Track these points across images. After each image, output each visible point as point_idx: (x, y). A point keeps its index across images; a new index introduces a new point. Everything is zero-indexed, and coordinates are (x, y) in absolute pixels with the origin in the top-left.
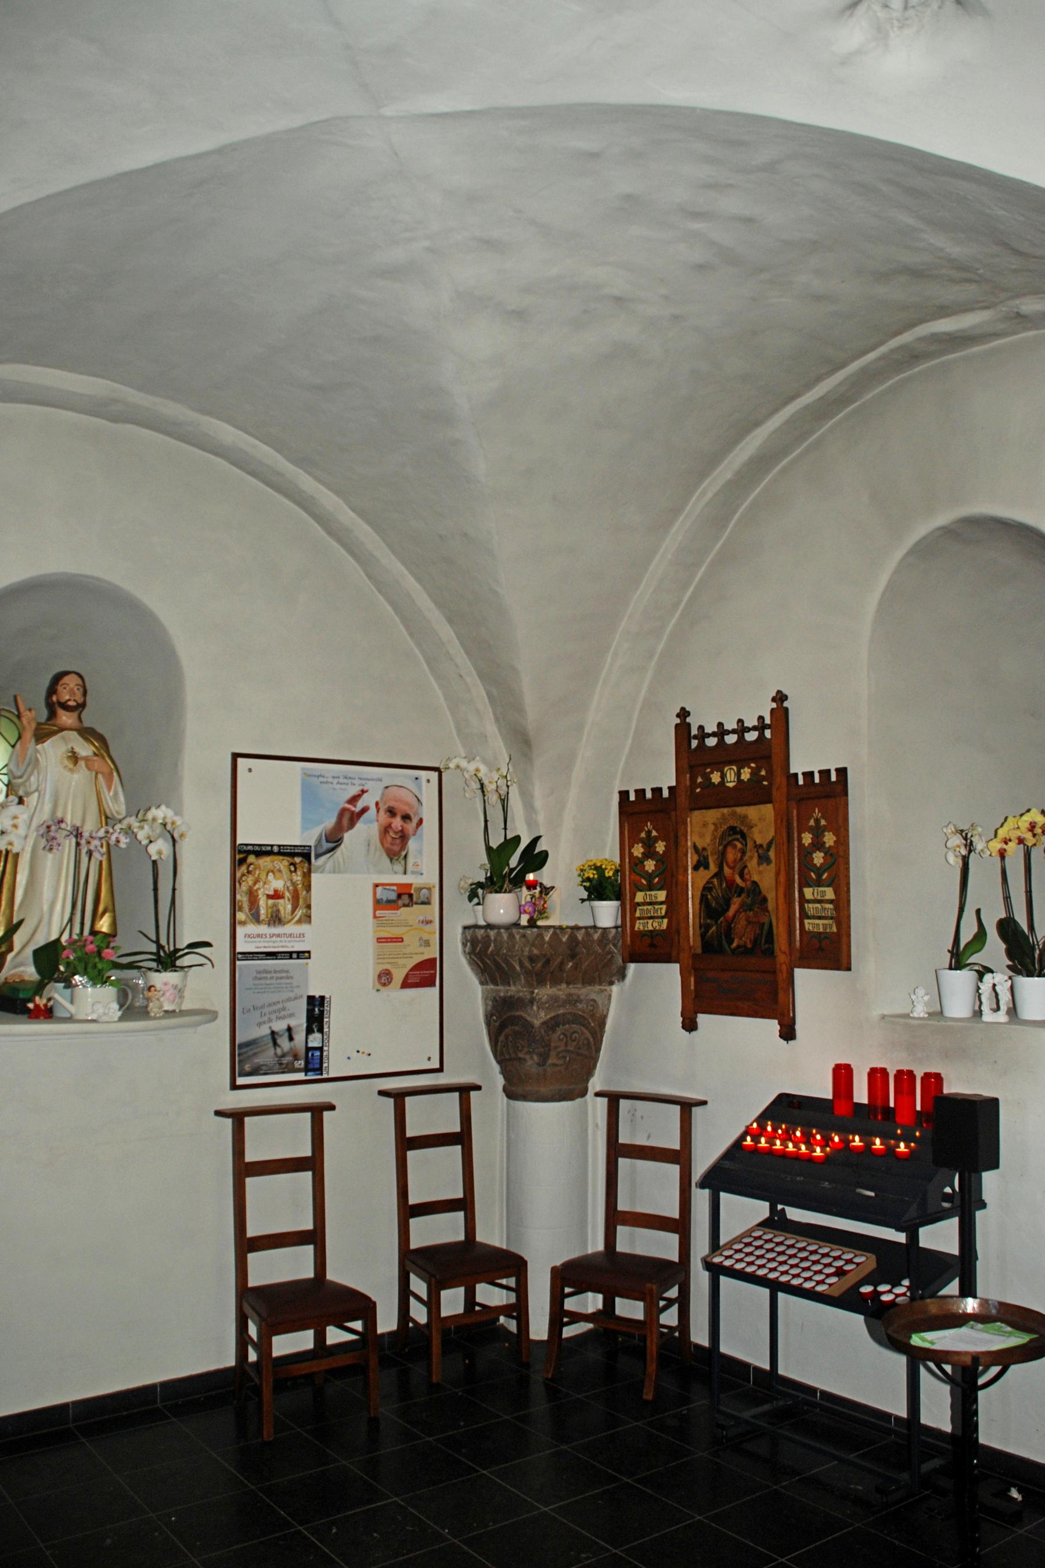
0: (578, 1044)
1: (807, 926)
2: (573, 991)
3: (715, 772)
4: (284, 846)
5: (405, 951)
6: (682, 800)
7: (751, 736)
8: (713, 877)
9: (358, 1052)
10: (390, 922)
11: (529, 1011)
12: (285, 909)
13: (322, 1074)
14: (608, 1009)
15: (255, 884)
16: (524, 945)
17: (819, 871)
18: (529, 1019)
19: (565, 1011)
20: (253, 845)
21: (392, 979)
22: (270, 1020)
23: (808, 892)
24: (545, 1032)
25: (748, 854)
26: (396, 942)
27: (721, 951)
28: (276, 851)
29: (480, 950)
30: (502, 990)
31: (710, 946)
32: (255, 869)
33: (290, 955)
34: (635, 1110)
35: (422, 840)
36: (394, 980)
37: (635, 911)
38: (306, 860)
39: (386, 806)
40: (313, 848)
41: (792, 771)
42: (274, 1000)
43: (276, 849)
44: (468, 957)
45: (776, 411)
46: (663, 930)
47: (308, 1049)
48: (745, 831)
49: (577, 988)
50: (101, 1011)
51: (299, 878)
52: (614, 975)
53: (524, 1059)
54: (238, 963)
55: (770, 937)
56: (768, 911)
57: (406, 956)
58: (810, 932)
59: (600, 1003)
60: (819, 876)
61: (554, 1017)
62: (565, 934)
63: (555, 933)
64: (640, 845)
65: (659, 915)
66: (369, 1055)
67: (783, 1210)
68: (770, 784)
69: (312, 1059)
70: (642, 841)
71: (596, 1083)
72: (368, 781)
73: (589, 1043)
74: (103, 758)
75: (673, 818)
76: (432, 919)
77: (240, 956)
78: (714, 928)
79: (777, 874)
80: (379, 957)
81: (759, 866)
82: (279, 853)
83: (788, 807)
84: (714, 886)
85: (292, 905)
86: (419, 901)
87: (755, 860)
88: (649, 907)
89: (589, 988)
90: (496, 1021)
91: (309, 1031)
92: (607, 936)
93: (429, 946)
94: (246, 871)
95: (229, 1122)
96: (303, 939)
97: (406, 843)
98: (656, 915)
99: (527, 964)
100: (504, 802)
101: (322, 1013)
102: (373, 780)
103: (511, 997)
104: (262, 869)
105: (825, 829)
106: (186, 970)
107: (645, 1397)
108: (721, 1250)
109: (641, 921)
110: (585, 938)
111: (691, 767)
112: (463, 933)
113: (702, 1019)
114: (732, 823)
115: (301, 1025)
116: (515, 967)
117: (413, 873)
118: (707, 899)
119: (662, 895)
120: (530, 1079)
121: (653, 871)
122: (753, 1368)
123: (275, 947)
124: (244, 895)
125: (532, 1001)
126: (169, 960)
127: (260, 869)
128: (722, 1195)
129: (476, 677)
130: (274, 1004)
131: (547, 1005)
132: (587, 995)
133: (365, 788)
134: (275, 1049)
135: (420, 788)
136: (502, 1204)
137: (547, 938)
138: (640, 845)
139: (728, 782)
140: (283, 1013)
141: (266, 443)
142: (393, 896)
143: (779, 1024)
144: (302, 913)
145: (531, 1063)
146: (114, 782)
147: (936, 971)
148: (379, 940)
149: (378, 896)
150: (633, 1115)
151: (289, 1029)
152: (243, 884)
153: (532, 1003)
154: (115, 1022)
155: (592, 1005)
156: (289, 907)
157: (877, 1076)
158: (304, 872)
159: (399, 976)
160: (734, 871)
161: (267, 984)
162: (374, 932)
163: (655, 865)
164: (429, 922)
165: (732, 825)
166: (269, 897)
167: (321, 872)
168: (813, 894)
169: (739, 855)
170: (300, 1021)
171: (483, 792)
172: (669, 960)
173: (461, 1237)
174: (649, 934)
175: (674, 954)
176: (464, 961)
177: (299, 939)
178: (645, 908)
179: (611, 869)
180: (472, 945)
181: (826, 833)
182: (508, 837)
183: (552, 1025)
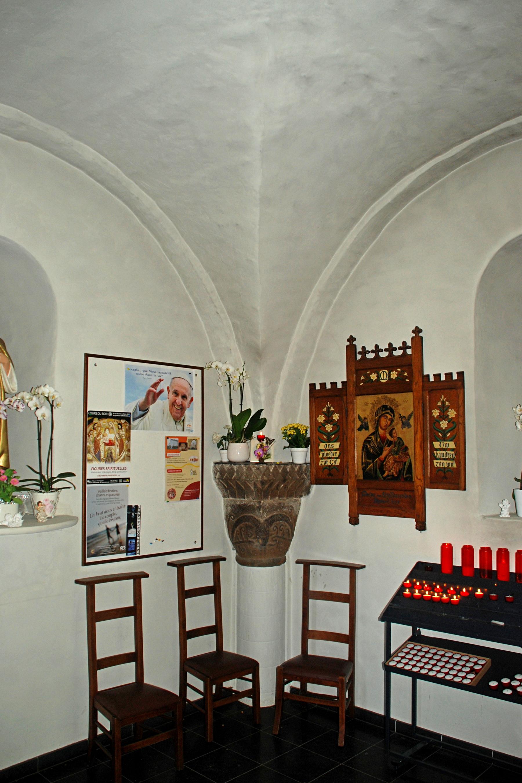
1: (435, 464)
2: (281, 501)
3: (373, 374)
4: (115, 412)
5: (183, 478)
6: (351, 389)
7: (398, 353)
8: (371, 435)
9: (157, 539)
10: (175, 460)
11: (257, 513)
12: (115, 452)
13: (136, 554)
14: (299, 511)
15: (98, 436)
16: (258, 474)
17: (444, 432)
18: (256, 518)
19: (277, 513)
20: (97, 412)
21: (175, 494)
22: (106, 521)
23: (436, 445)
24: (267, 526)
25: (395, 422)
26: (178, 472)
27: (376, 478)
28: (110, 416)
29: (226, 477)
30: (239, 501)
31: (367, 475)
32: (98, 426)
33: (118, 480)
34: (316, 570)
36: (176, 495)
37: (319, 454)
38: (128, 422)
39: (173, 390)
40: (132, 414)
41: (425, 373)
42: (109, 509)
43: (110, 414)
44: (217, 481)
45: (424, 162)
46: (337, 466)
47: (128, 539)
48: (393, 408)
49: (284, 499)
50: (11, 520)
51: (124, 433)
52: (303, 491)
53: (253, 542)
54: (87, 485)
55: (410, 470)
56: (409, 456)
57: (183, 481)
58: (437, 468)
59: (295, 508)
60: (444, 435)
62: (281, 467)
63: (275, 467)
64: (323, 415)
65: (335, 456)
66: (163, 541)
67: (419, 630)
68: (411, 381)
69: (131, 545)
70: (324, 413)
71: (291, 555)
72: (163, 374)
73: (289, 531)
74: (4, 353)
75: (345, 400)
76: (198, 458)
77: (89, 481)
78: (371, 465)
79: (415, 434)
80: (168, 481)
81: (402, 428)
82: (112, 417)
83: (423, 393)
84: (372, 440)
85: (119, 449)
86: (191, 448)
87: (400, 425)
88: (328, 452)
89: (290, 499)
90: (233, 519)
91: (129, 527)
92: (302, 469)
94: (92, 428)
95: (84, 587)
96: (126, 470)
97: (184, 412)
98: (333, 456)
99: (259, 485)
100: (242, 388)
101: (136, 516)
102: (166, 373)
103: (244, 505)
104: (102, 426)
105: (448, 407)
106: (59, 490)
107: (339, 745)
108: (393, 657)
109: (323, 460)
110: (291, 470)
111: (357, 371)
112: (214, 466)
113: (362, 518)
114: (384, 403)
115: (124, 524)
116: (250, 488)
117: (188, 430)
118: (367, 448)
119: (337, 445)
121: (331, 431)
122: (397, 722)
123: (108, 476)
124: (91, 443)
125: (259, 508)
126: (47, 485)
127: (100, 426)
128: (393, 624)
129: (226, 314)
130: (108, 511)
131: (268, 510)
132: (288, 504)
133: (162, 378)
134: (109, 539)
135: (191, 378)
136: (234, 626)
137: (271, 470)
138: (323, 415)
139: (382, 379)
140: (113, 517)
141: (112, 162)
142: (176, 444)
143: (416, 521)
144: (125, 454)
145: (257, 544)
146: (10, 370)
147: (513, 490)
148: (169, 471)
149: (168, 445)
150: (315, 573)
151: (117, 527)
152: (91, 436)
154: (20, 527)
156: (118, 450)
157: (486, 552)
158: (126, 429)
159: (179, 493)
160: (386, 431)
161: (104, 499)
162: (166, 466)
164: (196, 460)
165: (385, 404)
166: (106, 444)
167: (136, 430)
168: (440, 445)
169: (389, 422)
170: (123, 522)
171: (229, 382)
172: (341, 483)
173: (214, 649)
174: (328, 468)
175: (345, 480)
176: (214, 483)
177: (123, 470)
178: (326, 452)
179: (304, 429)
180: (220, 474)
181: (449, 410)
183: (270, 521)
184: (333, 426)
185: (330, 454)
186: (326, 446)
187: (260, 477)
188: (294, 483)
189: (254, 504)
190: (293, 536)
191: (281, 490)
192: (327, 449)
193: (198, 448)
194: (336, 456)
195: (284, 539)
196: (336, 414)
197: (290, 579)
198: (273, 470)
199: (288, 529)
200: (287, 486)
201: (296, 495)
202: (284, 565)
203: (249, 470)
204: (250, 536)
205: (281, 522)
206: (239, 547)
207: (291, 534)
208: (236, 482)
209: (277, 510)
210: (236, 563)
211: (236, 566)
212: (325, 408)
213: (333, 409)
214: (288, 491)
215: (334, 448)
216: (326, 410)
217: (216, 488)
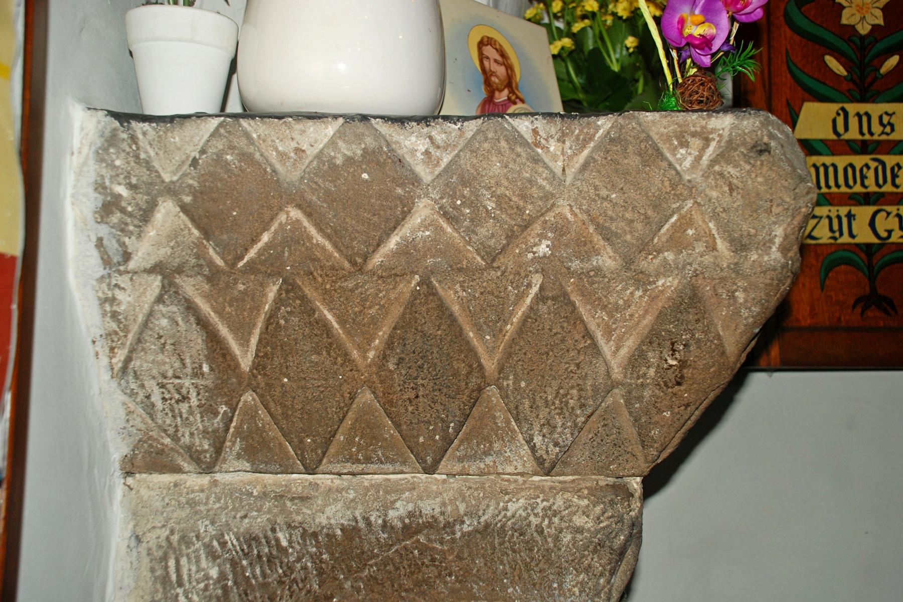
88: (859, 161)
98: (888, 188)
178: (841, 161)
185: (871, 174)
186: (840, 121)
189: (551, 514)
192: (848, 142)
200: (521, 408)
203: (634, 161)
215: (894, 136)
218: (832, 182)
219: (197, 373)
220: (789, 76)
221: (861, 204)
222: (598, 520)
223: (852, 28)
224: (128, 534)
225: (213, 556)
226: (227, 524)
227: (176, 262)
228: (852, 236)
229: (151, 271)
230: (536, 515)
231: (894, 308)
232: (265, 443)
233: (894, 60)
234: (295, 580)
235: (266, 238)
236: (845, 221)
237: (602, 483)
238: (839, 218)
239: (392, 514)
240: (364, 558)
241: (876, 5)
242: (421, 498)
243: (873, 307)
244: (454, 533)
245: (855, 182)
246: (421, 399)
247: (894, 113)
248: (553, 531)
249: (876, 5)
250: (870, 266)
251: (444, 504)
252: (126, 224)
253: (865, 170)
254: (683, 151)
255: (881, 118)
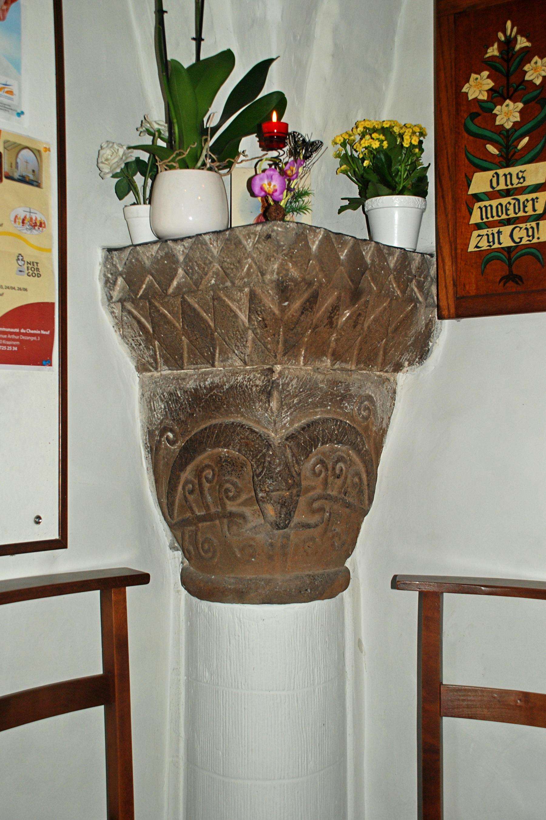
0: (344, 482)
2: (341, 376)
14: (390, 418)
24: (293, 455)
35: (19, 33)
44: (117, 311)
52: (406, 349)
53: (243, 517)
59: (378, 404)
61: (308, 426)
65: (530, 212)
73: (360, 479)
76: (43, 219)
86: (16, 176)
88: (504, 201)
90: (172, 443)
92: (409, 264)
93: (39, 276)
98: (521, 214)
109: (484, 232)
116: (236, 316)
120: (252, 556)
137: (314, 248)
138: (486, 73)
153: (269, 395)
155: (367, 408)
163: (521, 112)
178: (494, 203)
180: (128, 281)
182: (202, 57)
184: (525, 103)
185: (511, 208)
186: (494, 180)
187: (276, 266)
188: (385, 309)
189: (250, 380)
190: (371, 500)
191: (342, 328)
193: (44, 184)
194: (534, 210)
195: (348, 505)
196: (536, 58)
197: (359, 644)
198: (320, 247)
199: (358, 474)
201: (384, 360)
202: (342, 599)
203: (233, 247)
204: (231, 494)
205: (338, 450)
206: (194, 542)
207: (366, 492)
208: (184, 301)
209: (326, 406)
210: (184, 592)
211: (183, 603)
212: (496, 46)
213: (528, 44)
214: (364, 342)
216: (496, 53)
217: (115, 337)
218: (489, 215)
219: (140, 336)
220: (466, 161)
221: (505, 225)
222: (263, 382)
223: (502, 126)
224: (140, 394)
225: (162, 401)
226: (164, 389)
227: (124, 298)
228: (500, 243)
229: (118, 302)
230: (246, 381)
231: (522, 281)
232: (168, 359)
233: (526, 139)
234: (183, 409)
235: (144, 286)
236: (496, 236)
237: (265, 368)
238: (493, 234)
239: (207, 383)
240: (201, 399)
241: (516, 110)
242: (214, 377)
243: (511, 281)
244: (223, 389)
245: (502, 213)
246: (199, 339)
247: (525, 171)
248: (250, 387)
249: (516, 110)
250: (509, 259)
251: (220, 379)
252: (110, 287)
253: (508, 205)
254: (249, 240)
255: (518, 174)
